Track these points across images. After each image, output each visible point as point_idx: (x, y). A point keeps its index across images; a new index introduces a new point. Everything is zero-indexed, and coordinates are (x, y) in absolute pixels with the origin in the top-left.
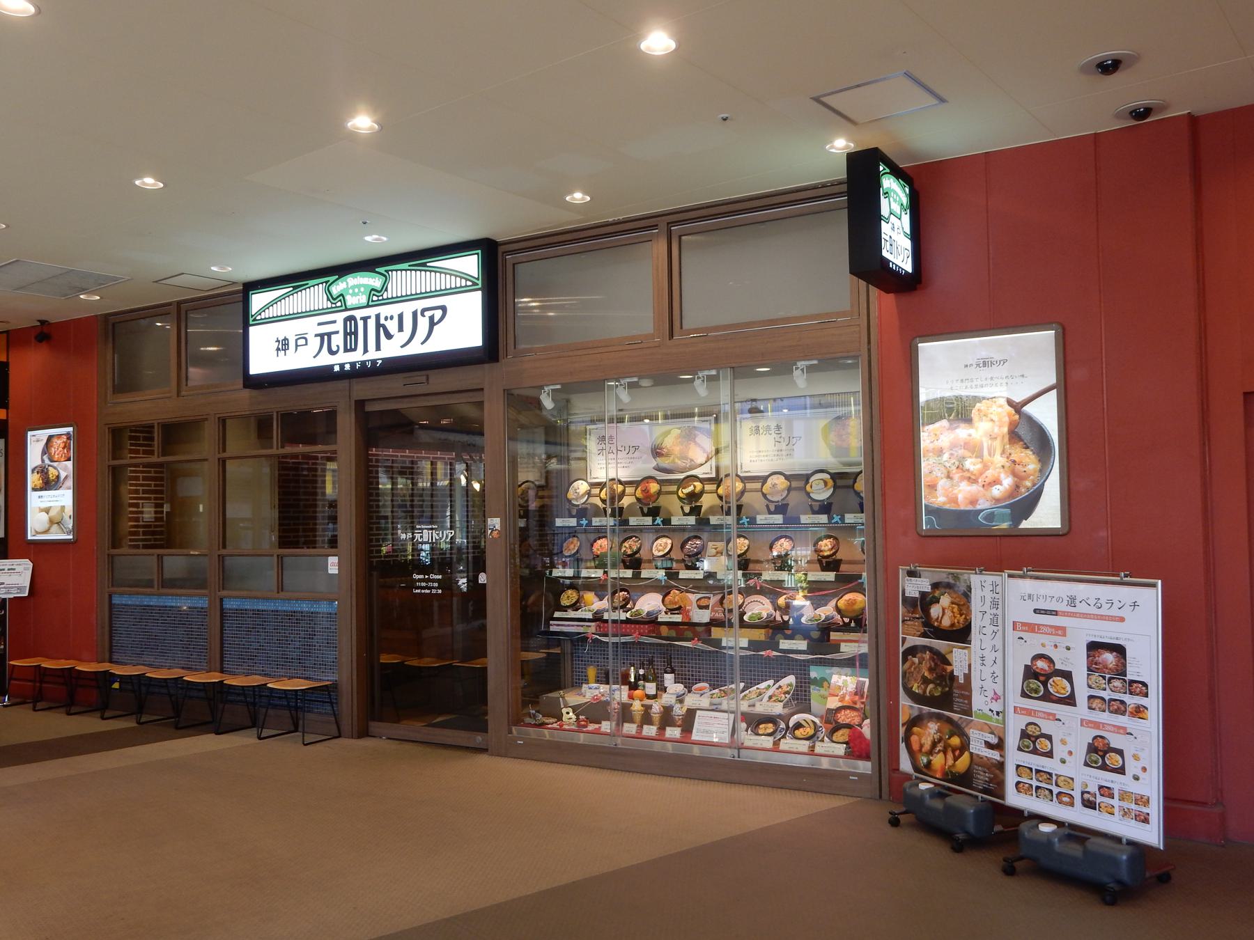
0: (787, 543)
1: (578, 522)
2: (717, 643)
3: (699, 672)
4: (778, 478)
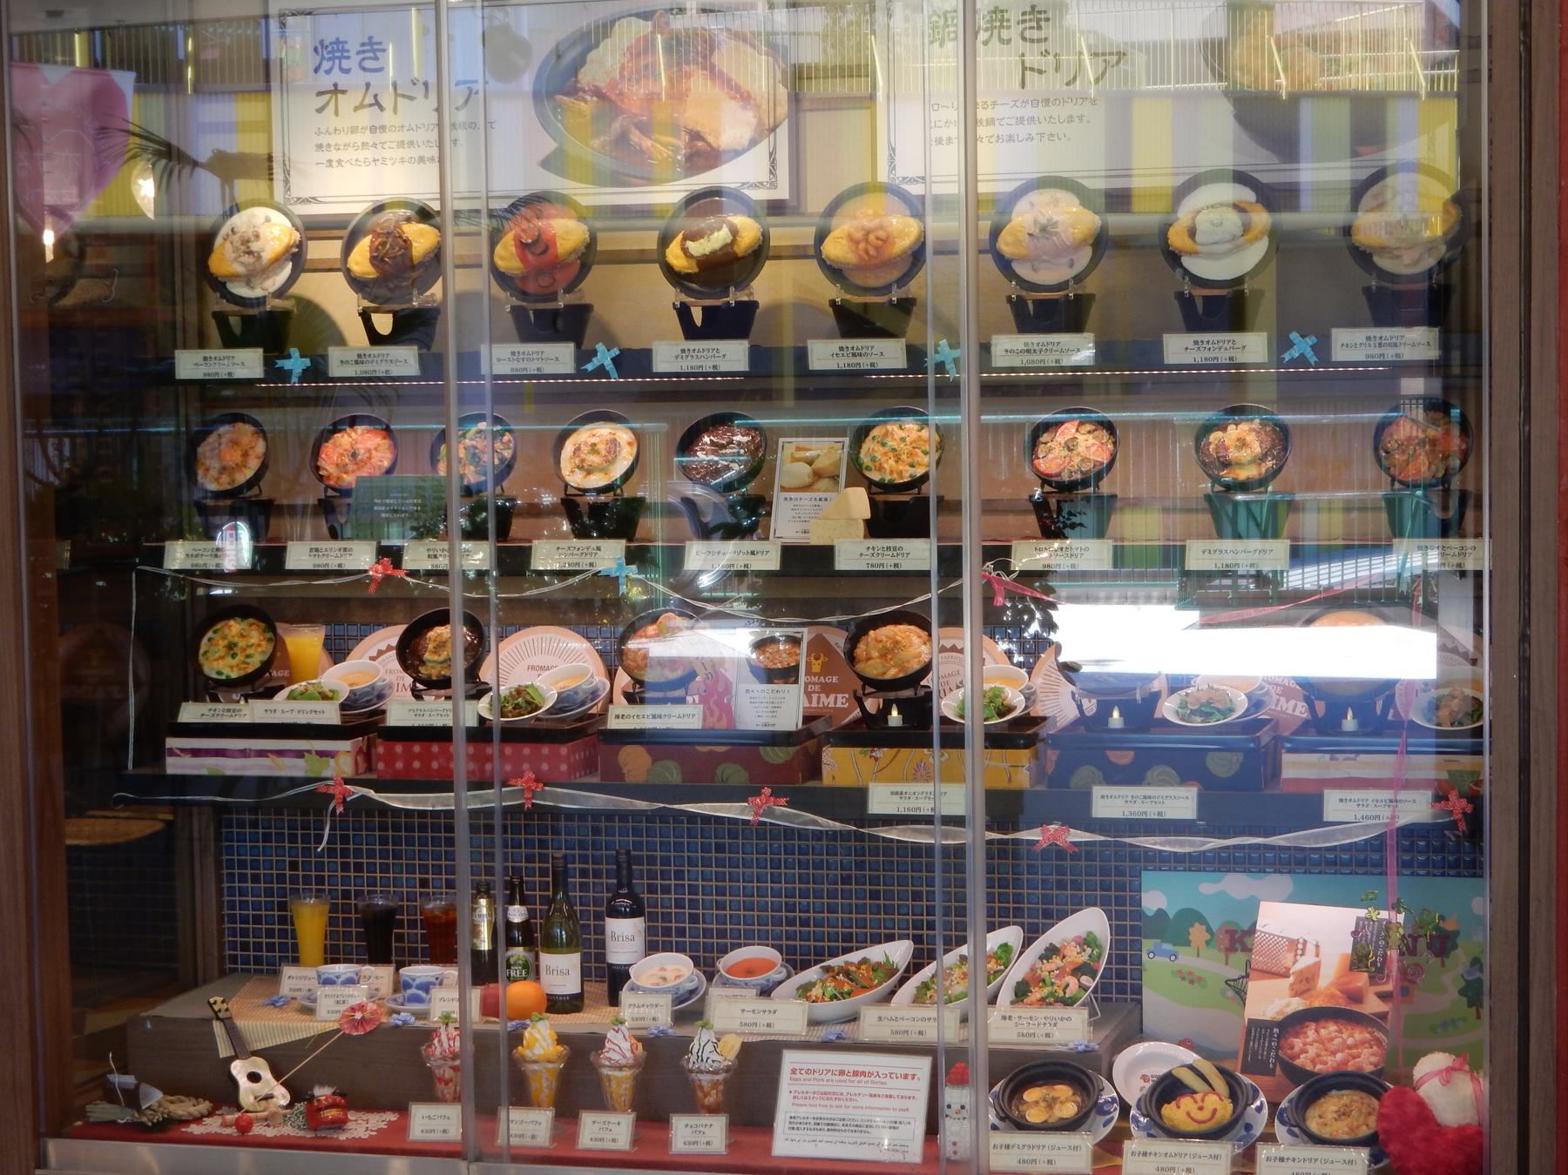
0: (1091, 440)
1: (268, 363)
2: (851, 802)
3: (720, 906)
4: (1056, 202)
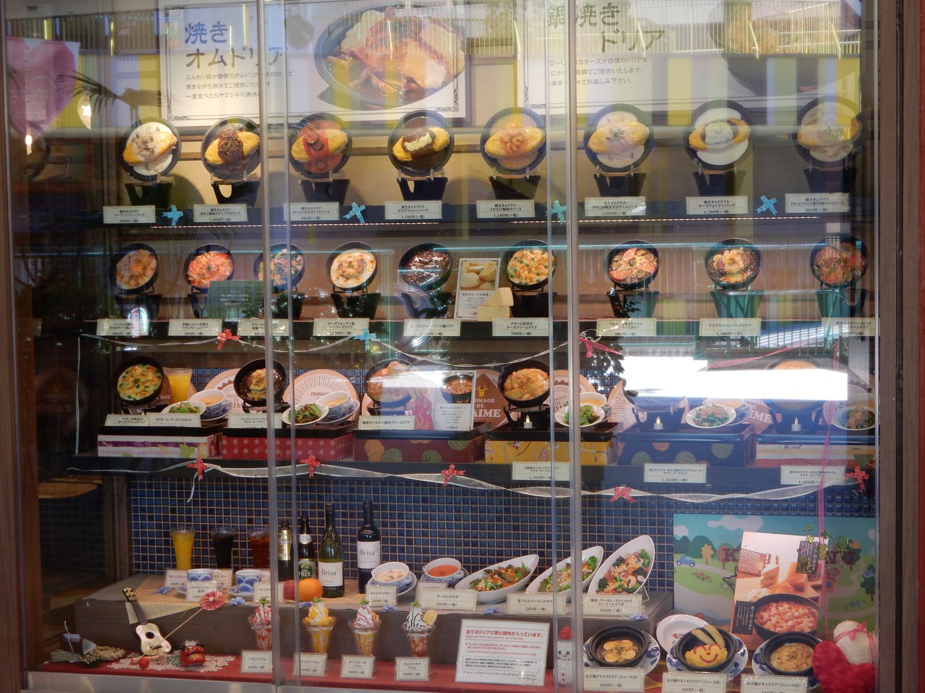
0: (643, 259)
1: (158, 214)
2: (502, 473)
4: (623, 119)
